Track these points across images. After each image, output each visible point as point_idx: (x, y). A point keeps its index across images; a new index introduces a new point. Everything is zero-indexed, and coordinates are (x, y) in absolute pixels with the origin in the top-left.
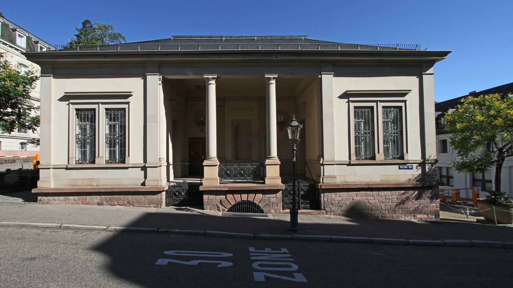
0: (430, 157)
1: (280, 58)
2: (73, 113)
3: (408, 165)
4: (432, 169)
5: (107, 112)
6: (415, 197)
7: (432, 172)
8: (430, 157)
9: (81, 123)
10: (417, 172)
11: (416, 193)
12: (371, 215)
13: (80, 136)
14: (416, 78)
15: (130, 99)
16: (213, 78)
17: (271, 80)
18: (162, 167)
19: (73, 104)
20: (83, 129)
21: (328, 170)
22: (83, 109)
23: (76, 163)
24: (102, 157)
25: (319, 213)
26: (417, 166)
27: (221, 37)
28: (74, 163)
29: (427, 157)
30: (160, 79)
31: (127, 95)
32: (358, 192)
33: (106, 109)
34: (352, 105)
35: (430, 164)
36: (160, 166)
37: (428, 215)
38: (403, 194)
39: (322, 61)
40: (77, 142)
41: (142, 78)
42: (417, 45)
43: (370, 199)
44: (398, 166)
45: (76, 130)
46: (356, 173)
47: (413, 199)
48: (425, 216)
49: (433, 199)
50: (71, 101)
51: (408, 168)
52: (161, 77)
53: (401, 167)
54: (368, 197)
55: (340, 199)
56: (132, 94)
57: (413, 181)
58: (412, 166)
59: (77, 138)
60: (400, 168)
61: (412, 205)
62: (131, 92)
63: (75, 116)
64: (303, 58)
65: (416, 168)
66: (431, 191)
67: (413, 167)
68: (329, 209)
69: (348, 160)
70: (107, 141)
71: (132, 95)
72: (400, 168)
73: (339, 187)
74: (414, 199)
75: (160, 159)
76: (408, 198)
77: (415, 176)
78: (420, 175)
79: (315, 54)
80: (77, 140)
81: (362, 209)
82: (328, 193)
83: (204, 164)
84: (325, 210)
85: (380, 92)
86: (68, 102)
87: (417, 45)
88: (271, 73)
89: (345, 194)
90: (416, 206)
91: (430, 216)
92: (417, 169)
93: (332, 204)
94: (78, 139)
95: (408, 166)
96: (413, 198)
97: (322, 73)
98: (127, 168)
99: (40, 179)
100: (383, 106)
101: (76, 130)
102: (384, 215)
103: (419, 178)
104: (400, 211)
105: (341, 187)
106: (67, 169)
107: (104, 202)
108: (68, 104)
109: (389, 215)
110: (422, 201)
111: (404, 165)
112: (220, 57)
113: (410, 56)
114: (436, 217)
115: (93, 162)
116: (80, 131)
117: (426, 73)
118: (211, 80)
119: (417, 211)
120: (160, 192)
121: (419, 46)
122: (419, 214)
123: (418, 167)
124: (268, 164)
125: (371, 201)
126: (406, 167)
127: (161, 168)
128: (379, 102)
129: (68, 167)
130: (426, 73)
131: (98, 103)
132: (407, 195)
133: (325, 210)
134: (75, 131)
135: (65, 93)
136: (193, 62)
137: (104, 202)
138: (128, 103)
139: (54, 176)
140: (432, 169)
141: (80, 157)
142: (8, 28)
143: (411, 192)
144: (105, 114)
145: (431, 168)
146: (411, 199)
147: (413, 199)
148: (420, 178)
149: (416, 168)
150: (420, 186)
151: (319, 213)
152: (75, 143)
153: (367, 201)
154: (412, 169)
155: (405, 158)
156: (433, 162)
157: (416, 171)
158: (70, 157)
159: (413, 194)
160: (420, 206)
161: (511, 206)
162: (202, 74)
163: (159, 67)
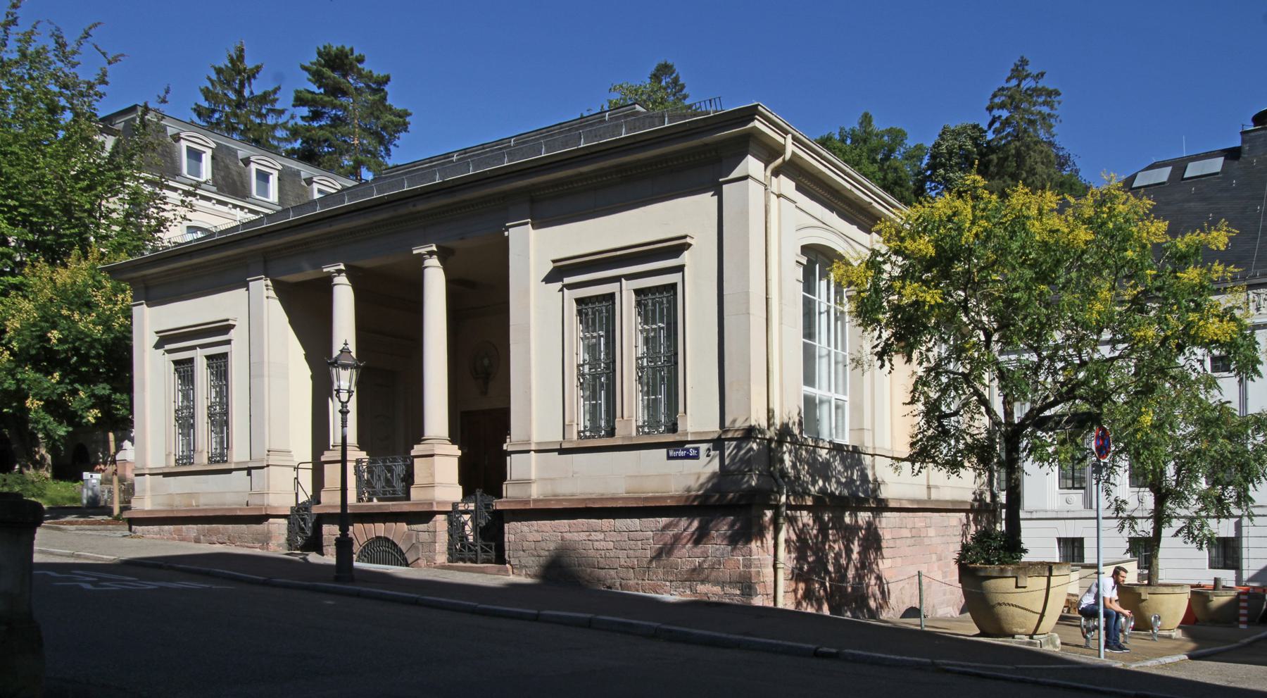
0: (734, 421)
1: (422, 206)
2: (572, 308)
3: (687, 446)
4: (737, 459)
5: (580, 308)
6: (693, 534)
7: (738, 465)
8: (734, 421)
9: (646, 327)
10: (704, 468)
11: (696, 524)
12: (599, 580)
13: (587, 367)
14: (712, 196)
15: (686, 257)
16: (431, 253)
17: (425, 259)
18: (435, 457)
19: (571, 287)
20: (592, 349)
21: (516, 466)
22: (597, 297)
23: (580, 437)
24: (629, 421)
25: (499, 571)
26: (709, 450)
27: (448, 155)
28: (206, 461)
29: (727, 424)
30: (267, 286)
31: (676, 247)
32: (571, 521)
33: (208, 357)
34: (571, 295)
35: (735, 443)
36: (268, 466)
37: (723, 588)
38: (666, 527)
39: (505, 196)
40: (581, 384)
41: (712, 193)
42: (710, 101)
43: (596, 538)
44: (665, 451)
45: (636, 347)
46: (577, 473)
47: (689, 540)
48: (717, 589)
49: (737, 544)
50: (567, 280)
51: (687, 457)
52: (269, 282)
53: (671, 453)
54: (592, 533)
55: (538, 537)
56: (688, 240)
57: (699, 491)
58: (697, 449)
59: (640, 368)
60: (669, 458)
61: (686, 557)
62: (685, 237)
63: (575, 318)
64: (403, 211)
65: (708, 456)
66: (732, 518)
67: (698, 453)
68: (517, 562)
69: (718, 429)
70: (640, 378)
71: (234, 326)
72: (669, 458)
73: (527, 507)
74: (691, 542)
75: (269, 451)
76: (677, 538)
77: (702, 480)
78: (714, 475)
79: (506, 176)
80: (582, 381)
81: (579, 565)
82: (517, 521)
83: (413, 453)
84: (509, 563)
85: (619, 253)
86: (559, 285)
87: (710, 101)
88: (425, 242)
89: (546, 525)
90: (697, 559)
91: (728, 590)
92: (709, 458)
93: (523, 551)
94: (583, 375)
95: (688, 450)
96: (689, 537)
97: (721, 180)
98: (229, 471)
99: (136, 494)
100: (635, 288)
101: (578, 354)
102: (625, 582)
103: (710, 485)
104: (660, 571)
105: (532, 506)
106: (562, 451)
107: (202, 537)
108: (561, 290)
109: (636, 581)
110: (710, 548)
111: (679, 449)
112: (331, 226)
113: (630, 149)
114: (742, 595)
115: (611, 433)
116: (587, 357)
117: (732, 176)
118: (335, 276)
119: (696, 575)
120: (261, 519)
121: (717, 100)
122: (703, 582)
123: (712, 453)
124: (420, 454)
125: (598, 543)
126: (682, 453)
127: (433, 464)
128: (626, 280)
129: (565, 446)
130: (732, 176)
131: (617, 279)
132: (676, 531)
133: (509, 563)
134: (575, 356)
135: (554, 261)
136: (305, 243)
137: (202, 537)
138: (680, 269)
139: (153, 489)
140: (737, 459)
141: (646, 418)
142: (297, 179)
143: (684, 522)
144: (634, 303)
145: (736, 454)
146: (685, 541)
147: (689, 540)
148: (713, 485)
149: (708, 456)
150: (696, 503)
151: (499, 571)
152: (575, 388)
153: (590, 543)
154: (696, 457)
155: (680, 428)
156: (738, 435)
157: (706, 465)
158: (567, 423)
159: (688, 527)
160: (704, 561)
161: (982, 574)
162: (318, 266)
163: (265, 262)
